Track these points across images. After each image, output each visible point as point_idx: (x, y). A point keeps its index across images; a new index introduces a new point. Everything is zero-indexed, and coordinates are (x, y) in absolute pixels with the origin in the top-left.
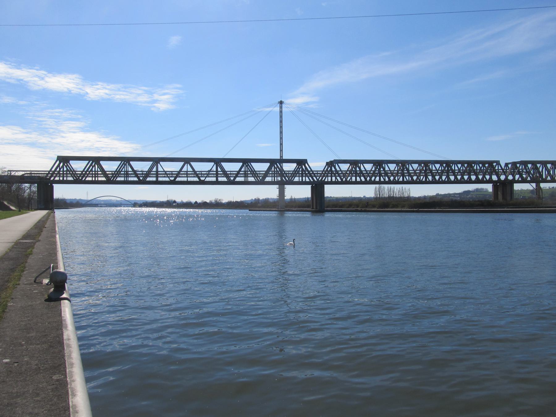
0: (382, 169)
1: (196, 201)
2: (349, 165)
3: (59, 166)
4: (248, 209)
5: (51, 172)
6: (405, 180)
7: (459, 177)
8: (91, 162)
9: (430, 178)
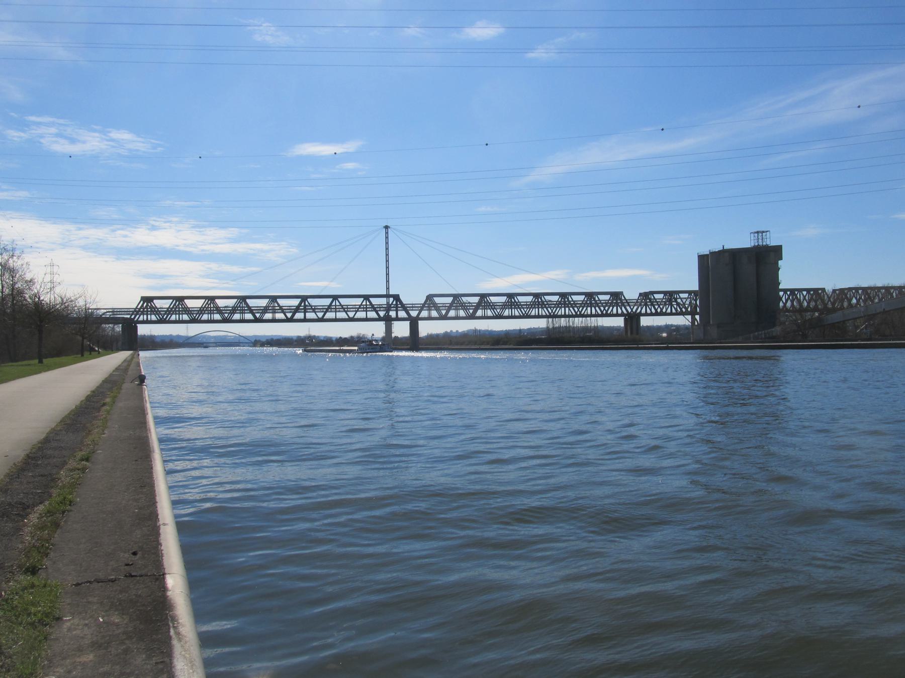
0: (566, 300)
2: (584, 296)
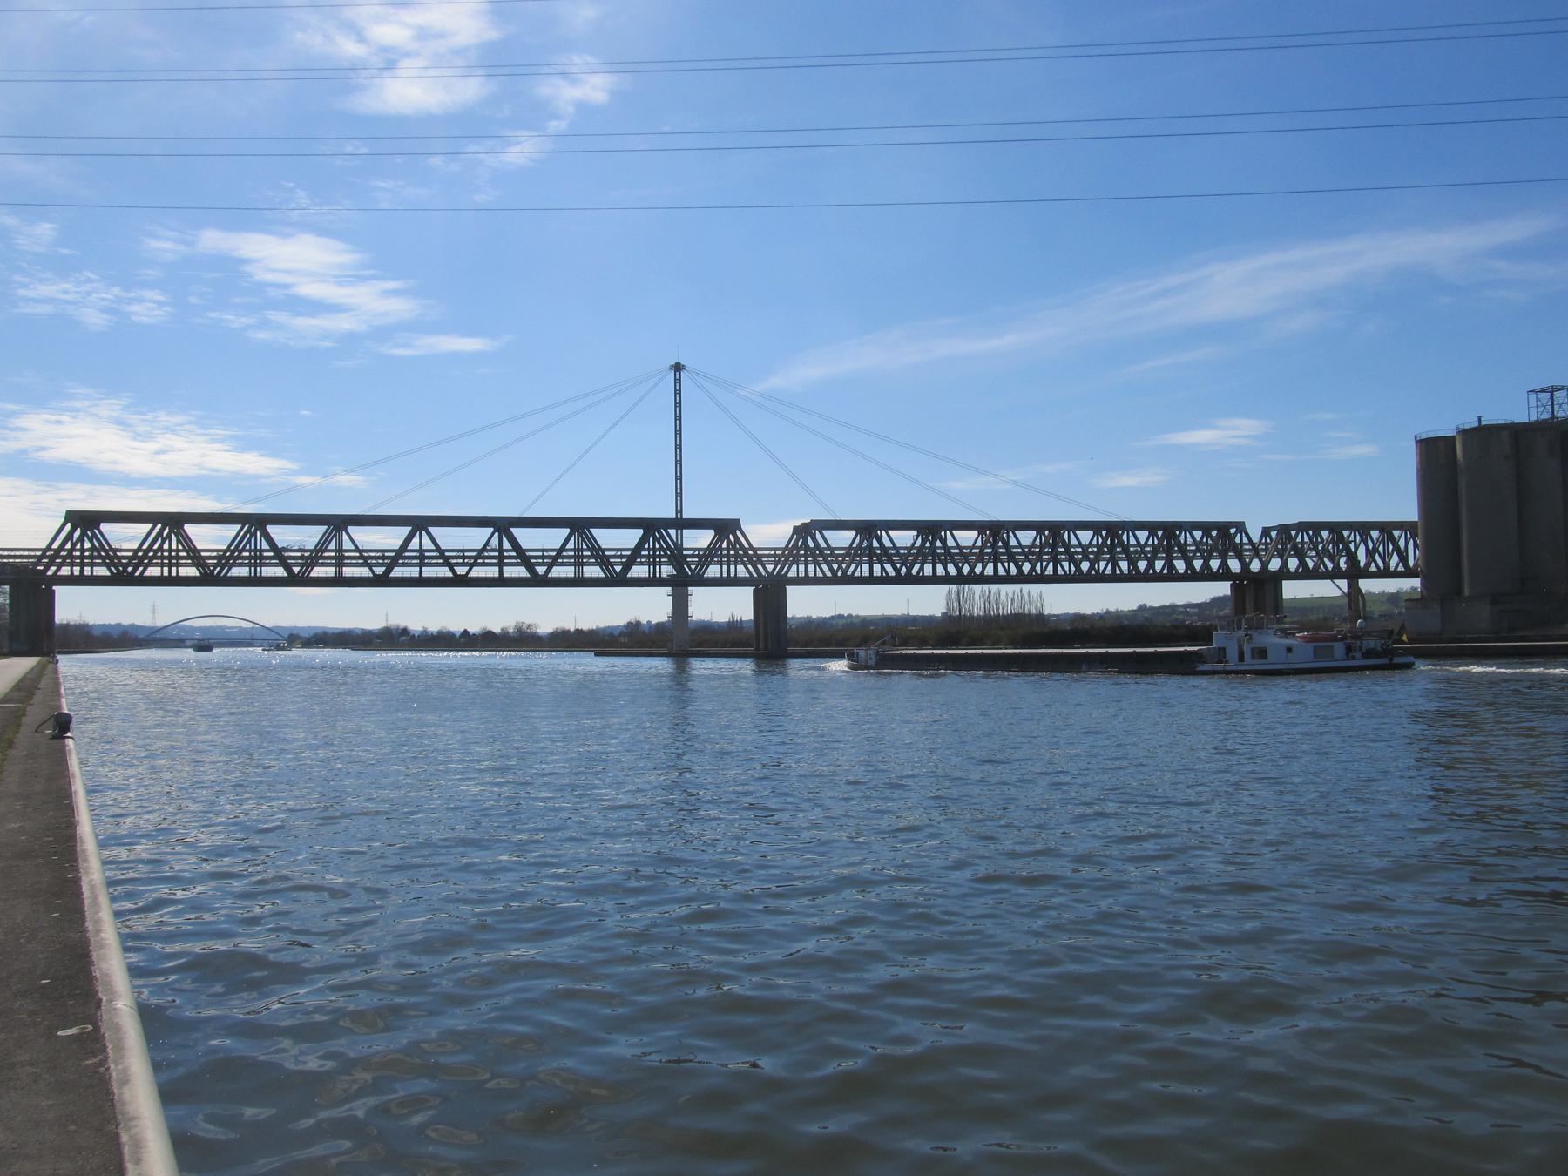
0: (938, 544)
1: (465, 630)
2: (854, 532)
3: (69, 537)
4: (592, 651)
5: (48, 554)
6: (1060, 572)
7: (1198, 564)
8: (159, 526)
9: (1124, 565)
